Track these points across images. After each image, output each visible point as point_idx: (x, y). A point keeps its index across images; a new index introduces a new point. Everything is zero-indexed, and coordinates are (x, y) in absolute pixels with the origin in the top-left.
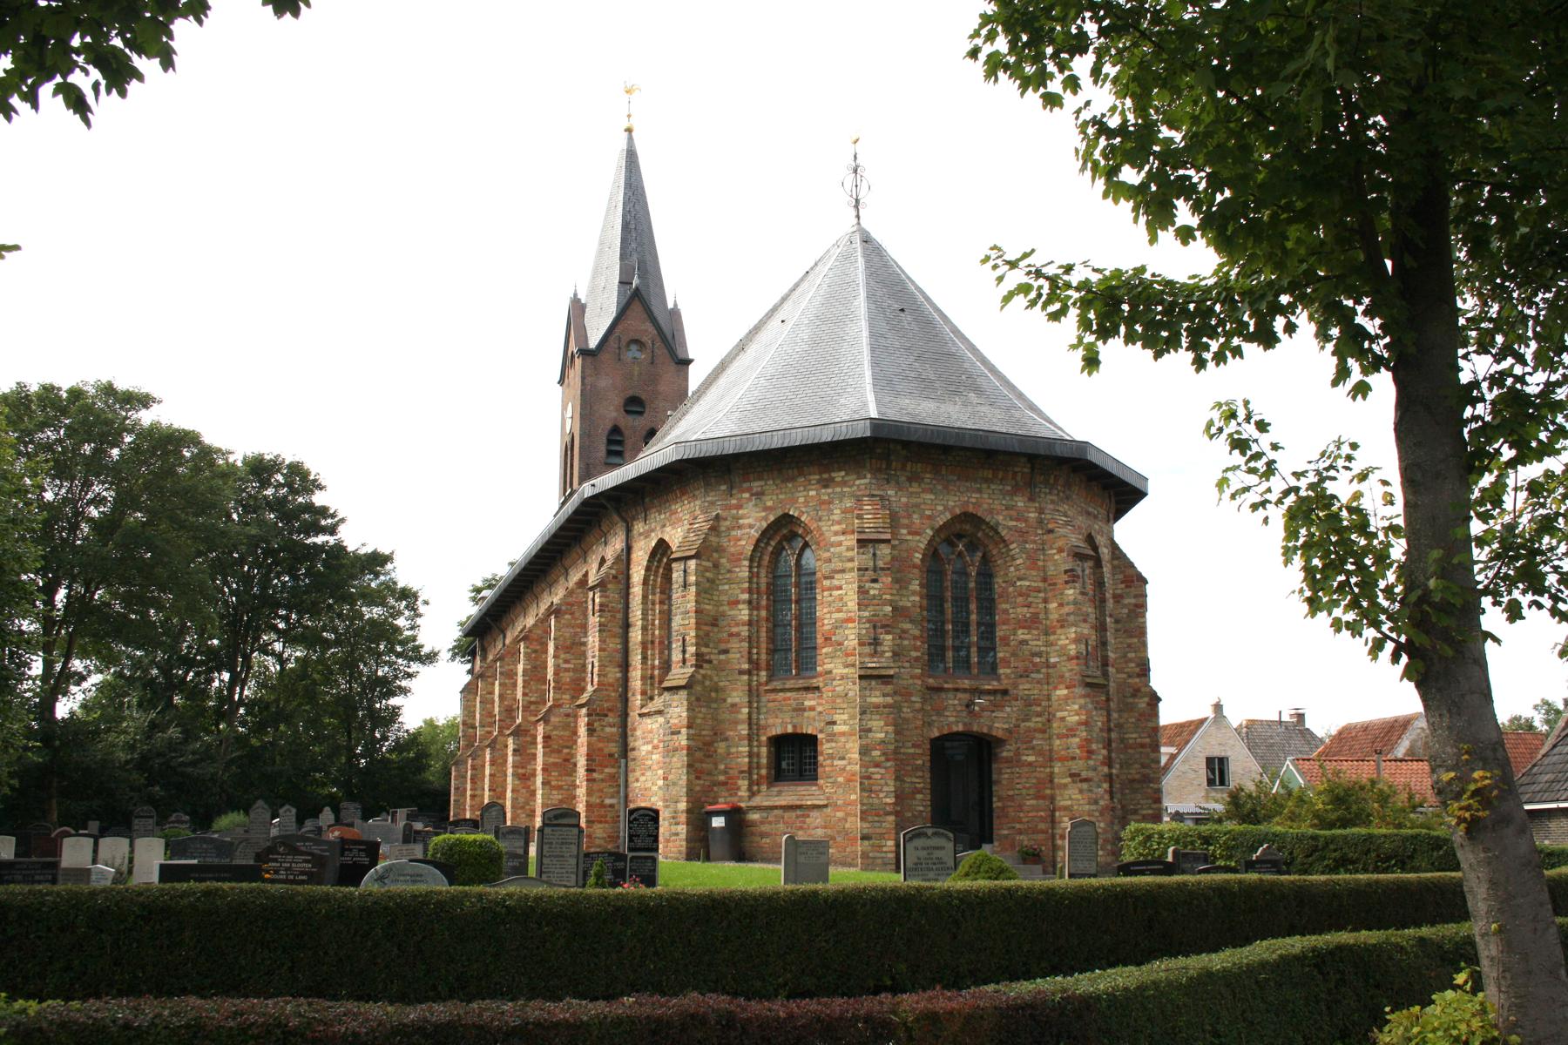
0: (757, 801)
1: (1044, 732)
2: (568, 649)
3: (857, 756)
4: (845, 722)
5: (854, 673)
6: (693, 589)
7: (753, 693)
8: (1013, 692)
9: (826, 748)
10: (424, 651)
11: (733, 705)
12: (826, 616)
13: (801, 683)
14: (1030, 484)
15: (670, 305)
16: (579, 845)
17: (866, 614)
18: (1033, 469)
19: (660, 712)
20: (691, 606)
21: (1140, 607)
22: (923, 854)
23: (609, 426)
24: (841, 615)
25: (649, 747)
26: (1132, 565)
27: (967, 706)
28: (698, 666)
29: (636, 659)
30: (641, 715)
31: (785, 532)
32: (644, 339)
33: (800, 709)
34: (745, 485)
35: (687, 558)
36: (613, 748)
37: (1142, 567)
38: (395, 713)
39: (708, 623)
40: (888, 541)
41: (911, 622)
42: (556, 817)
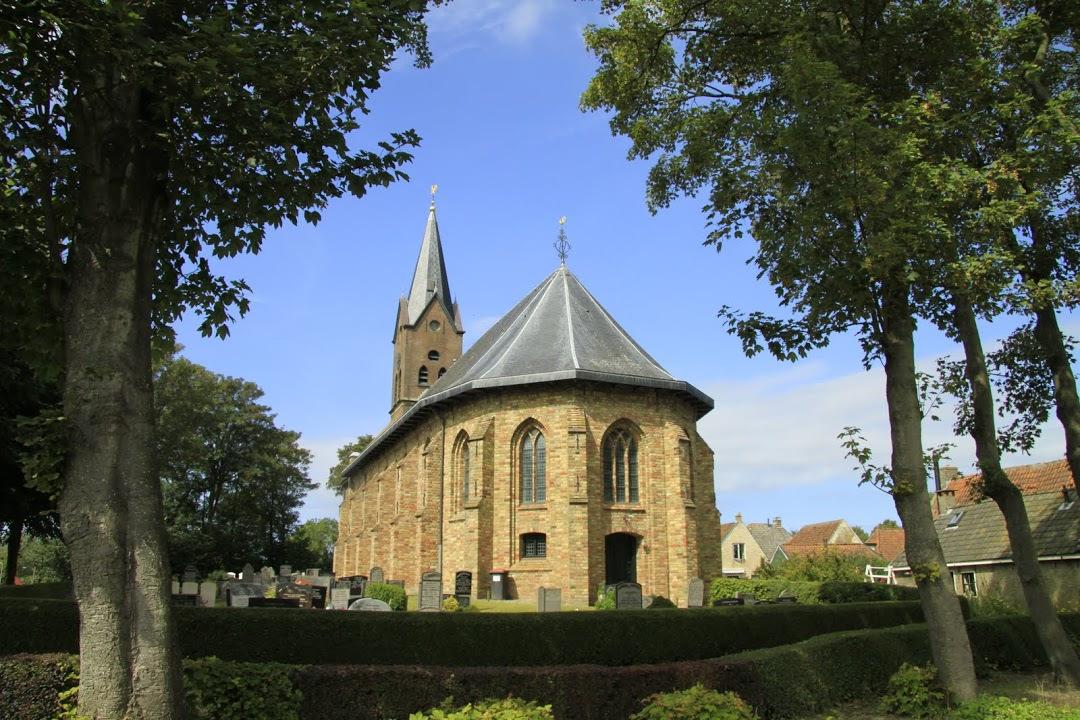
0: (514, 567)
1: (663, 532)
2: (408, 486)
3: (567, 544)
4: (561, 527)
5: (566, 501)
6: (482, 456)
7: (511, 511)
8: (647, 511)
9: (550, 540)
10: (313, 483)
11: (502, 517)
12: (551, 471)
13: (538, 506)
14: (657, 404)
15: (453, 302)
16: (441, 591)
17: (573, 470)
18: (657, 395)
19: (462, 521)
20: (481, 465)
21: (710, 467)
22: (626, 595)
23: (420, 365)
24: (561, 471)
25: (455, 539)
26: (706, 445)
27: (624, 519)
28: (484, 497)
29: (447, 492)
30: (450, 522)
31: (528, 426)
32: (439, 320)
33: (537, 520)
34: (509, 402)
35: (477, 440)
36: (436, 539)
37: (711, 445)
38: (294, 518)
39: (488, 473)
40: (584, 433)
41: (596, 474)
42: (429, 576)
